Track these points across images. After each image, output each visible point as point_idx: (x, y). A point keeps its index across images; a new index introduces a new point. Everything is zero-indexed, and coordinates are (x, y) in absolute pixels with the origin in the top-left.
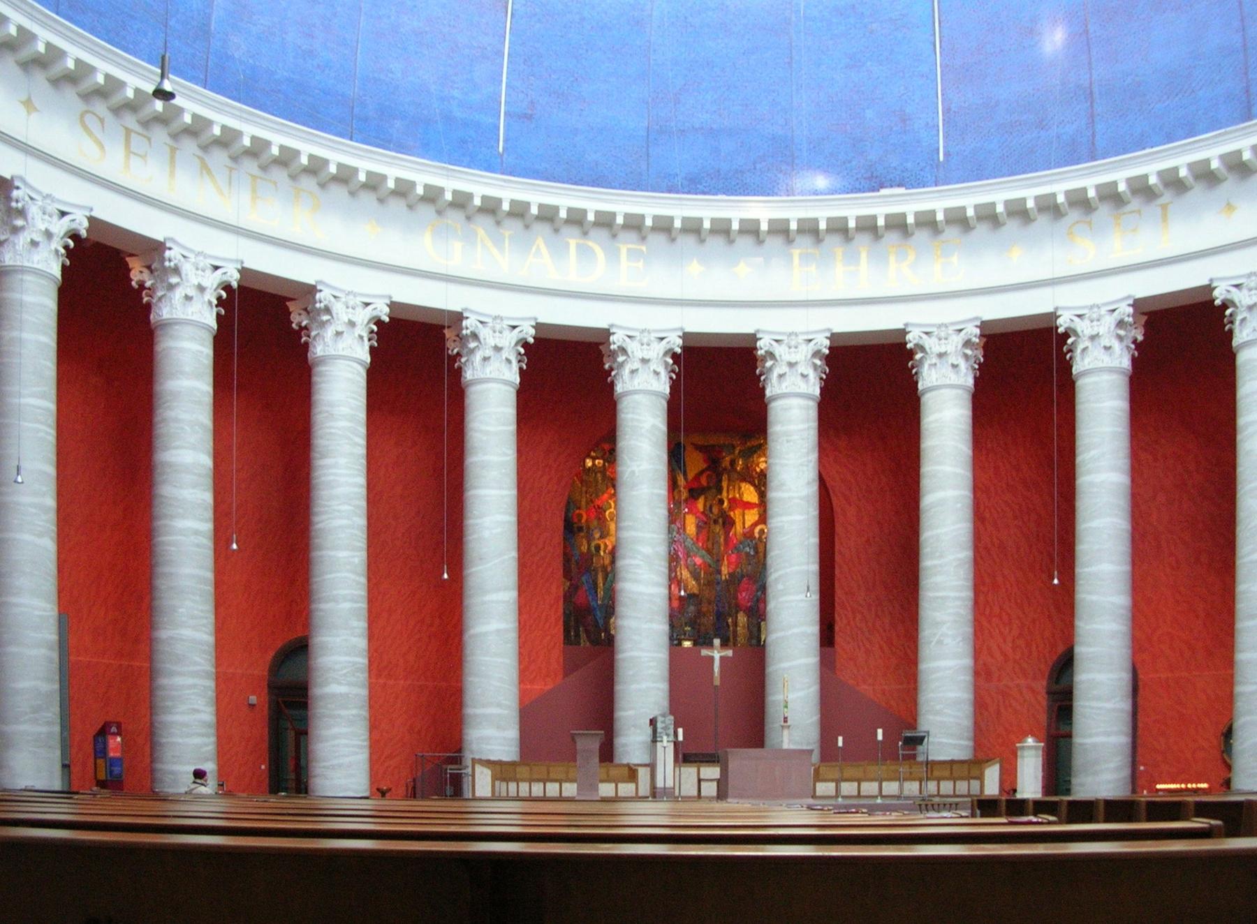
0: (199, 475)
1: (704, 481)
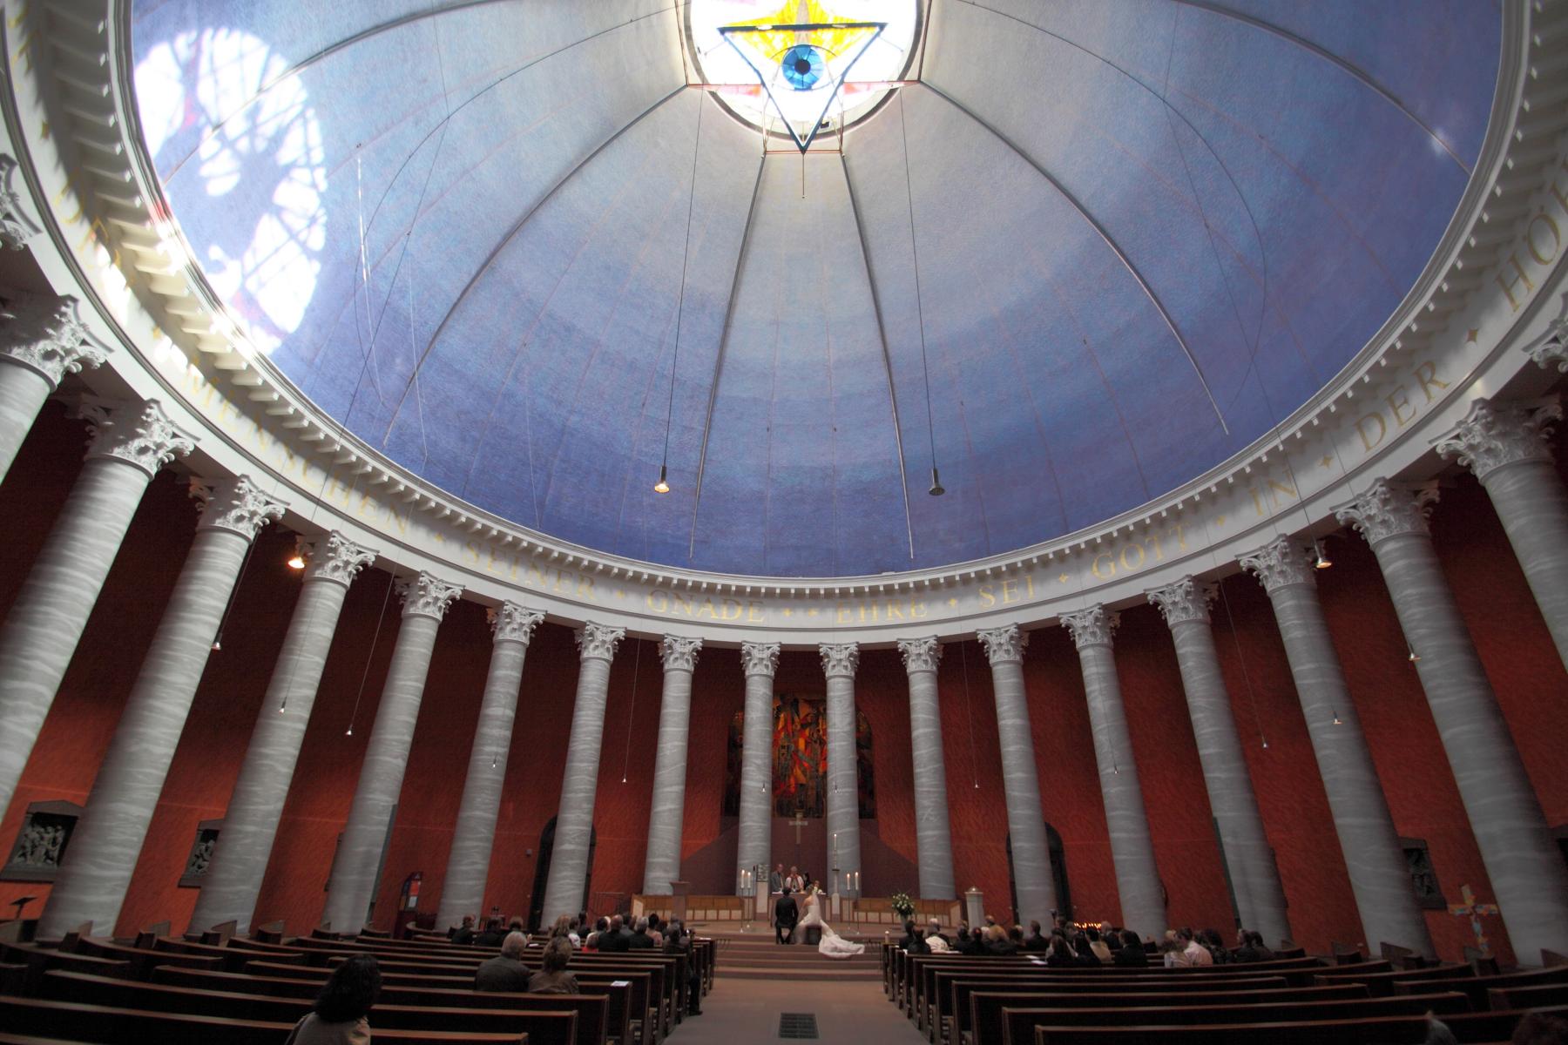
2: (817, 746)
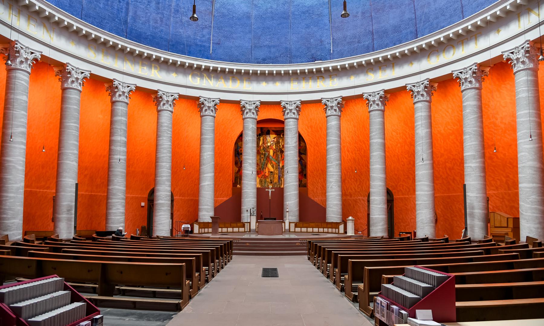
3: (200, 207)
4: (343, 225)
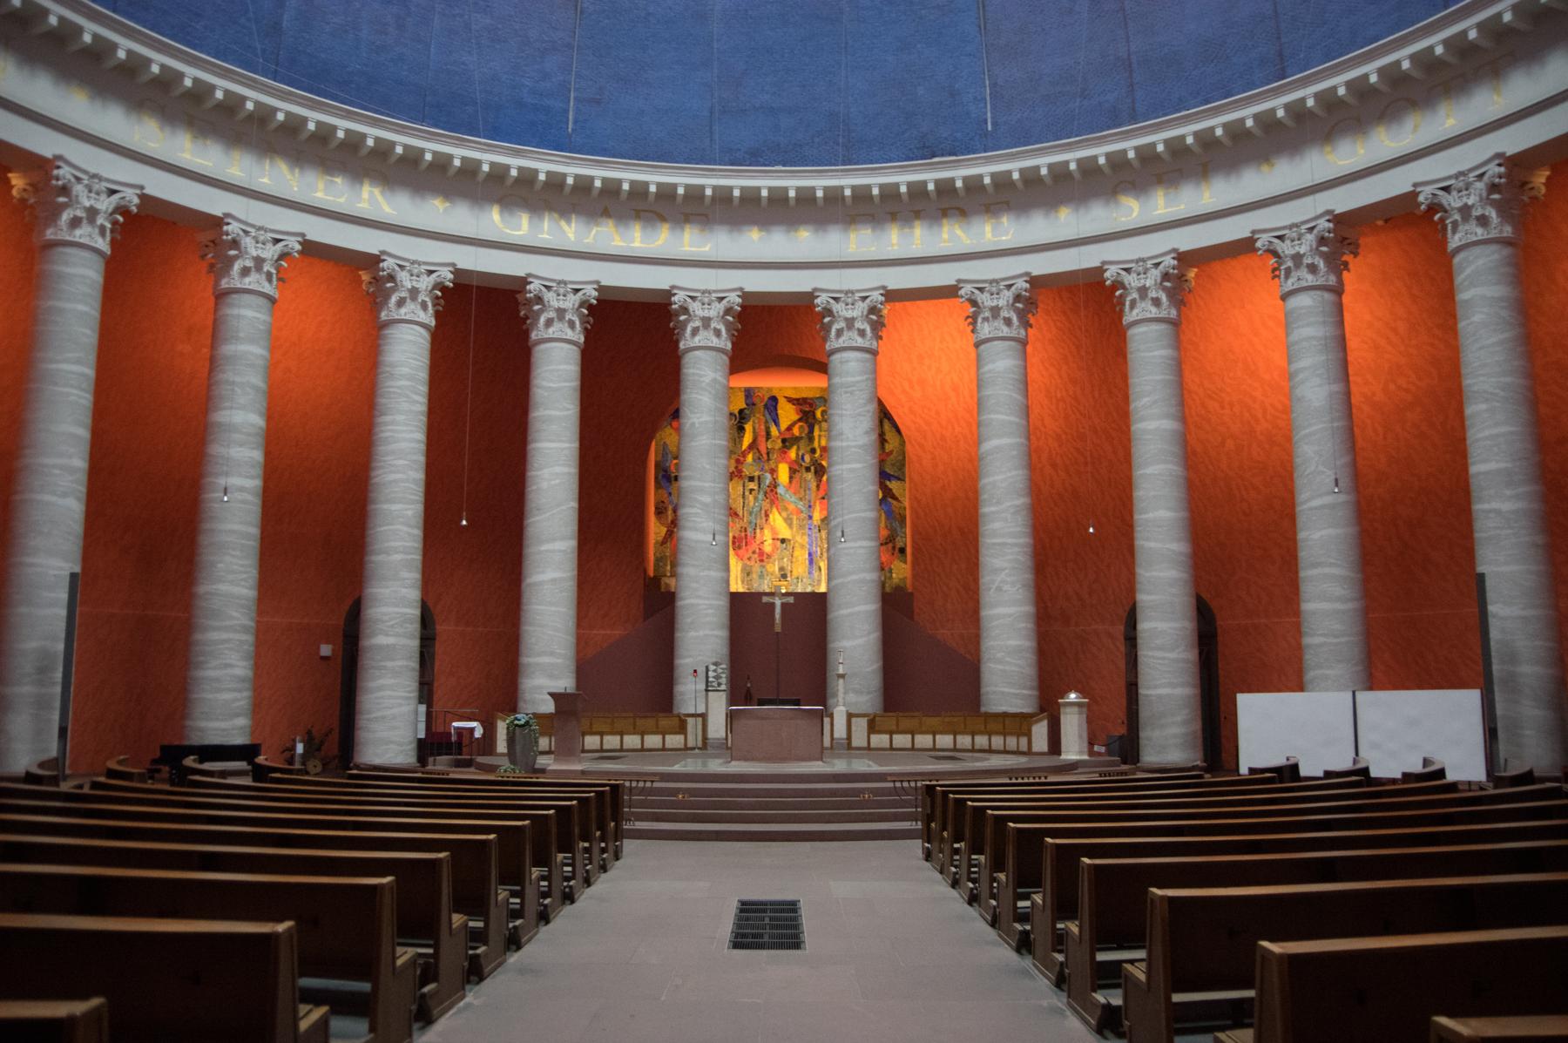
0: (249, 435)
1: (796, 431)
2: (810, 476)
3: (524, 660)
4: (1045, 723)
